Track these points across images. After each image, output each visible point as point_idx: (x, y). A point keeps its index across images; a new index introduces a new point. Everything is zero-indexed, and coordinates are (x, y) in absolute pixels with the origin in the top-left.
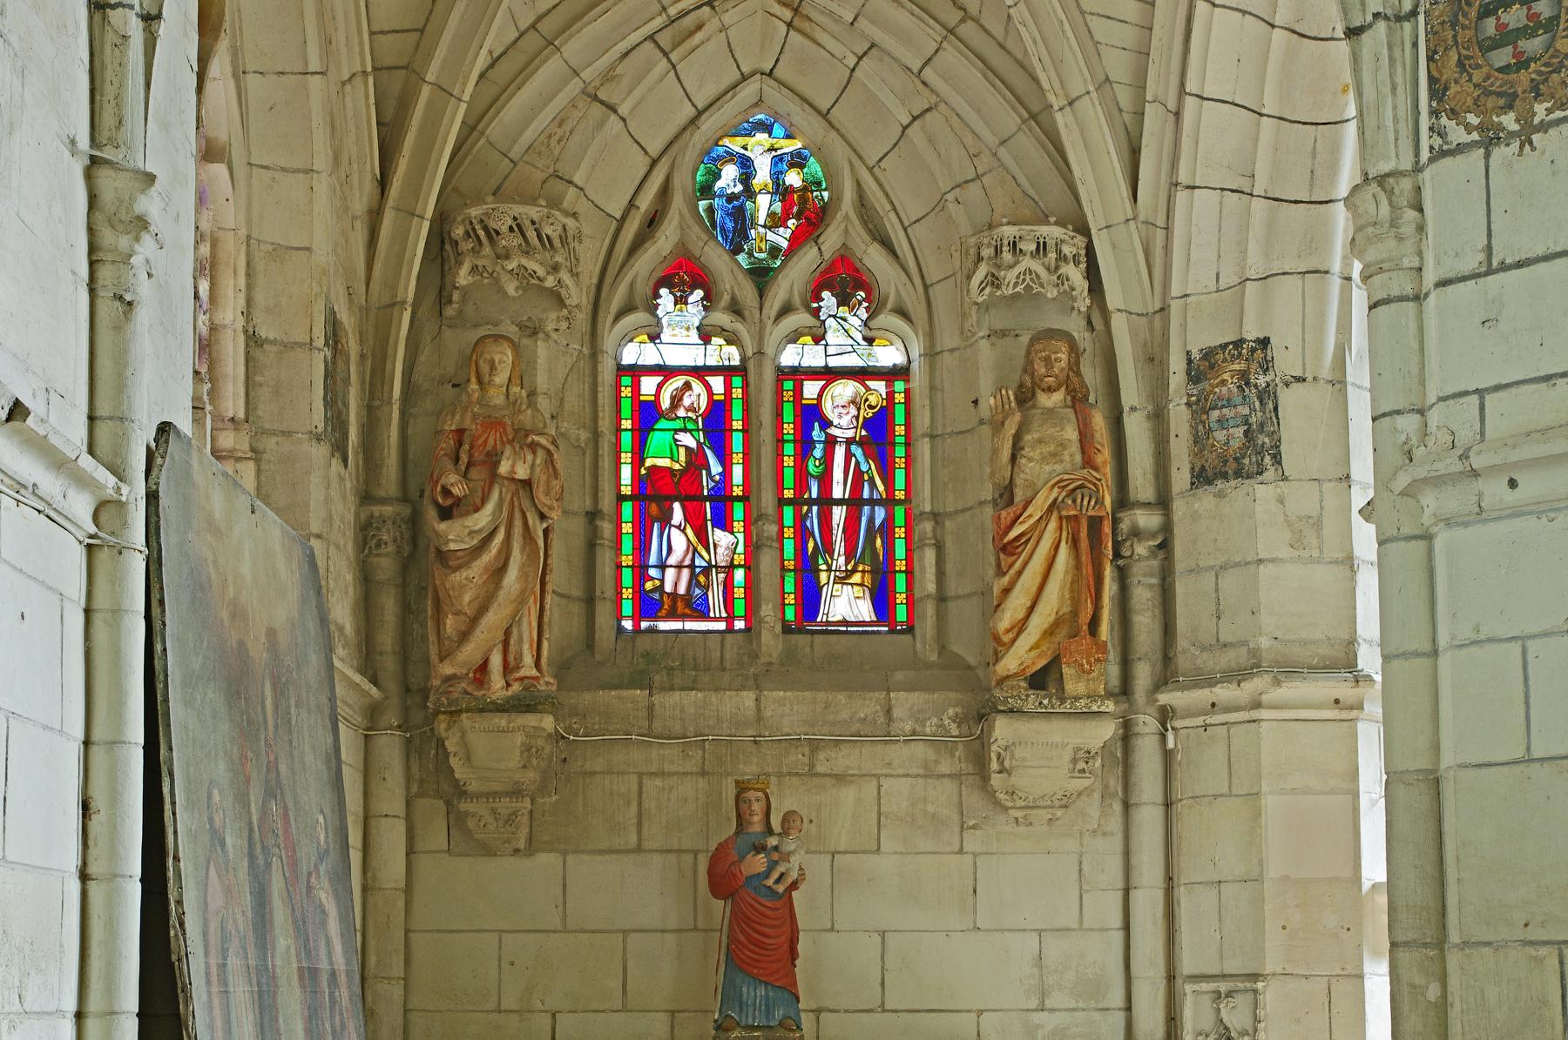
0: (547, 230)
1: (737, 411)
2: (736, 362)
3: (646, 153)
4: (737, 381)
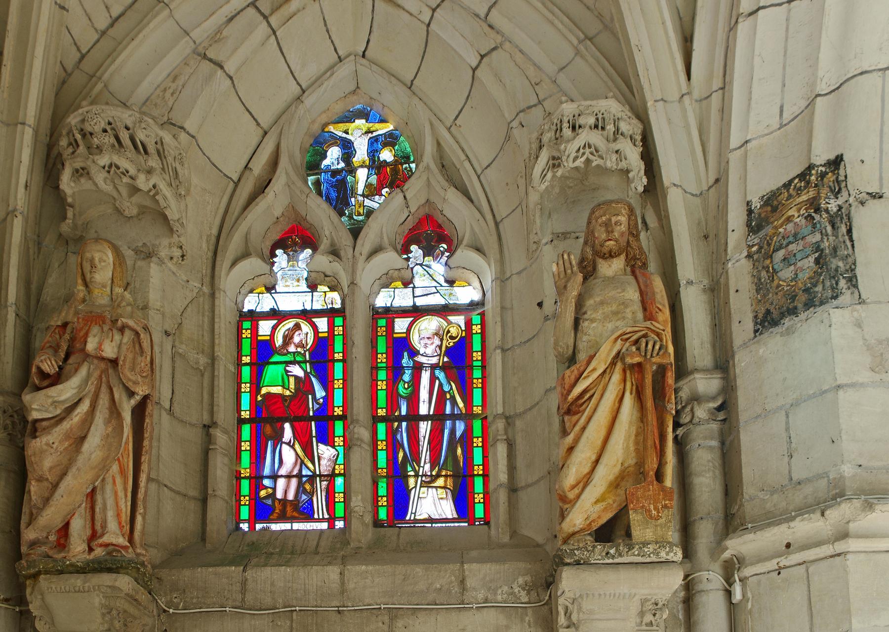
0: (140, 136)
1: (338, 346)
2: (338, 305)
3: (258, 124)
4: (338, 321)
